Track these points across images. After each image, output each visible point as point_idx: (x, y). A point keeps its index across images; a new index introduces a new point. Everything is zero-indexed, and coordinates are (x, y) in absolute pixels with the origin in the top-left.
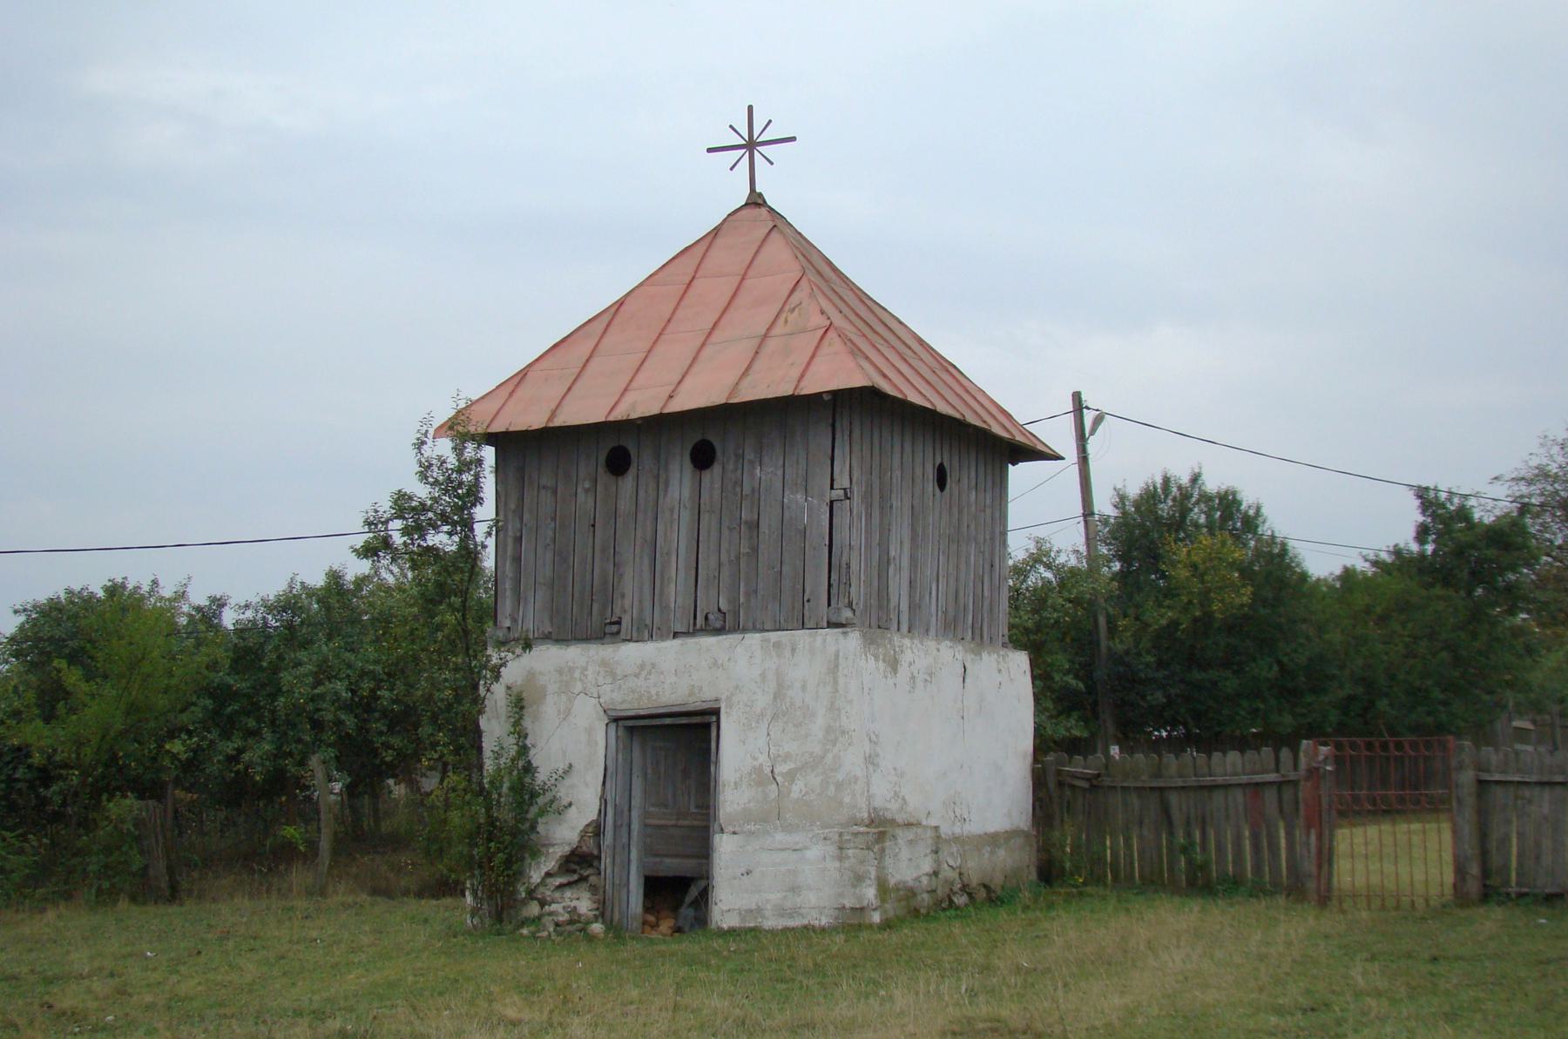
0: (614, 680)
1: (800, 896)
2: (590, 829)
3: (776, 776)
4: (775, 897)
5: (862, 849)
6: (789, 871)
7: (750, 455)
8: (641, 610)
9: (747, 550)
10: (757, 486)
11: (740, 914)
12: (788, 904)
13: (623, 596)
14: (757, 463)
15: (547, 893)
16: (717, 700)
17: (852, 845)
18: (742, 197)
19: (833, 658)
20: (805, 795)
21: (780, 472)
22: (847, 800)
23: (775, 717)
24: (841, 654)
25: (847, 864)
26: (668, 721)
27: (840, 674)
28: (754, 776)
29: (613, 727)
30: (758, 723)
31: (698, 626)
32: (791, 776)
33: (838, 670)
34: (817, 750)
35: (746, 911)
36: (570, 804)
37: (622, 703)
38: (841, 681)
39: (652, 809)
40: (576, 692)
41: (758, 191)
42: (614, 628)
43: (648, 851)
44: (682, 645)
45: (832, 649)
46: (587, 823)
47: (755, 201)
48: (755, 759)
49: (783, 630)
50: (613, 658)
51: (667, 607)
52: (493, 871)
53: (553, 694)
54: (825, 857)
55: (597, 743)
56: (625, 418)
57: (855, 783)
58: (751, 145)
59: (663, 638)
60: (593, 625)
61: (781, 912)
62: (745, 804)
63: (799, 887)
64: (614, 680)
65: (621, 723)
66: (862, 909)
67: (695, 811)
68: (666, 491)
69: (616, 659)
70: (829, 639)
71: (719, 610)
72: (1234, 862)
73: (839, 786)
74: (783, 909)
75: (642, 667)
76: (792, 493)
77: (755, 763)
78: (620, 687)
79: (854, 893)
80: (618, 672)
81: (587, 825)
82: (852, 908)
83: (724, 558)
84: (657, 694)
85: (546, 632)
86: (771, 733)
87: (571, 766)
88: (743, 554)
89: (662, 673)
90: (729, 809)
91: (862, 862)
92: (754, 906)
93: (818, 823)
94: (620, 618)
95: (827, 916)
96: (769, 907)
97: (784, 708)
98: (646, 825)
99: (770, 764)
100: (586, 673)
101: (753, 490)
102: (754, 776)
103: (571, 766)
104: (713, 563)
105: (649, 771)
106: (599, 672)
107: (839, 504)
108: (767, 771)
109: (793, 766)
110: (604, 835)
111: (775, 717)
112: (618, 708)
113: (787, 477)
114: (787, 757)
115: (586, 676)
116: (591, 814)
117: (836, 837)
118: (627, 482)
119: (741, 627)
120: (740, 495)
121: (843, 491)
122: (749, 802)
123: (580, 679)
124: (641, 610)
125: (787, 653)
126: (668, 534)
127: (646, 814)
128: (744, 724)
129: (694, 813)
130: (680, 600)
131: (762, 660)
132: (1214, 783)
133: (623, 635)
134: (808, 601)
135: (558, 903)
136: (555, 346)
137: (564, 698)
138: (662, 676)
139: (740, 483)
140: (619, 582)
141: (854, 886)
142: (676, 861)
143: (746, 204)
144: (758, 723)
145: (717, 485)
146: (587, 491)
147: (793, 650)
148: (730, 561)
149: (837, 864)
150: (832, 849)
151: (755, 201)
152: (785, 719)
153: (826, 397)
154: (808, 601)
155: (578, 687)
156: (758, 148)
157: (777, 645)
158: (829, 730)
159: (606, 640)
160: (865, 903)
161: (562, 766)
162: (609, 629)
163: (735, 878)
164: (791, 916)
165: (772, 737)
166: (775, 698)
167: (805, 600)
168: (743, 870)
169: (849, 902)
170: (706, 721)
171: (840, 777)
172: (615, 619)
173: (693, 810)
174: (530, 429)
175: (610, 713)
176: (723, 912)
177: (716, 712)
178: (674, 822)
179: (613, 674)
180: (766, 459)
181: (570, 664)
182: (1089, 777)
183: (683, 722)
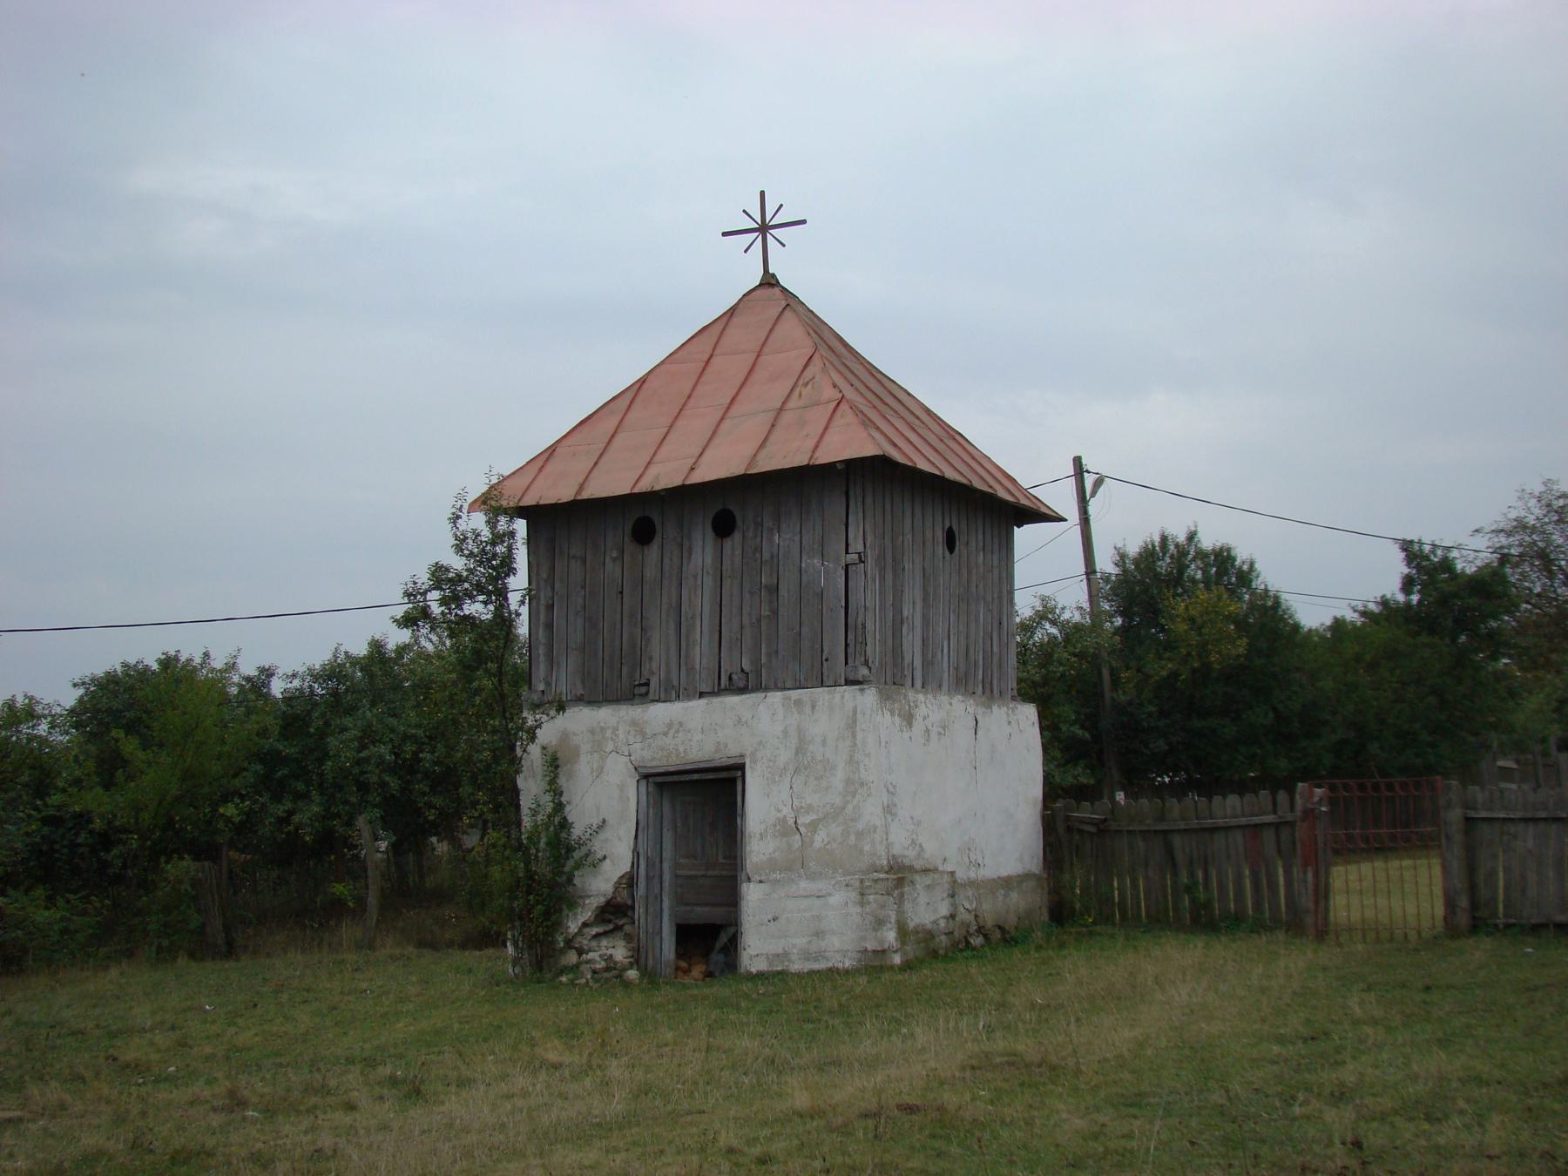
1: (823, 940)
2: (624, 881)
4: (801, 941)
5: (882, 894)
6: (813, 916)
7: (768, 523)
8: (668, 672)
9: (767, 613)
11: (768, 958)
13: (651, 659)
14: (776, 531)
15: (584, 942)
16: (742, 756)
17: (872, 891)
19: (851, 714)
20: (827, 844)
21: (797, 538)
24: (858, 711)
26: (696, 777)
27: (858, 728)
28: (778, 827)
29: (643, 783)
32: (813, 826)
34: (838, 801)
36: (605, 858)
37: (652, 760)
38: (859, 735)
40: (608, 750)
41: (771, 271)
42: (643, 690)
43: (679, 899)
45: (849, 706)
48: (779, 811)
49: (804, 688)
51: (693, 668)
55: (628, 799)
58: (764, 229)
59: (689, 697)
61: (807, 955)
66: (884, 951)
67: (724, 861)
68: (689, 563)
69: (645, 719)
71: (742, 670)
73: (859, 835)
75: (670, 726)
78: (649, 746)
83: (746, 621)
84: (685, 751)
87: (604, 821)
88: (764, 617)
90: (755, 859)
91: (882, 907)
92: (780, 951)
94: (649, 680)
95: (850, 959)
96: (795, 951)
97: (806, 762)
98: (677, 876)
99: (793, 815)
101: (772, 557)
102: (778, 827)
103: (604, 821)
108: (791, 822)
109: (815, 817)
115: (617, 736)
117: (857, 884)
118: (653, 551)
120: (759, 562)
121: (857, 555)
122: (774, 853)
123: (612, 739)
124: (668, 672)
125: (808, 709)
128: (768, 779)
133: (651, 696)
134: (827, 660)
137: (596, 756)
138: (689, 734)
140: (647, 646)
141: (875, 930)
142: (707, 909)
143: (760, 285)
145: (738, 552)
146: (614, 560)
147: (813, 707)
150: (854, 895)
151: (769, 281)
153: (839, 467)
154: (827, 660)
157: (798, 703)
158: (848, 782)
160: (886, 947)
161: (596, 822)
163: (762, 925)
164: (816, 959)
165: (795, 790)
166: (797, 753)
167: (824, 658)
169: (870, 946)
171: (860, 826)
172: (643, 681)
173: (721, 860)
178: (703, 873)
179: (642, 733)
181: (602, 724)
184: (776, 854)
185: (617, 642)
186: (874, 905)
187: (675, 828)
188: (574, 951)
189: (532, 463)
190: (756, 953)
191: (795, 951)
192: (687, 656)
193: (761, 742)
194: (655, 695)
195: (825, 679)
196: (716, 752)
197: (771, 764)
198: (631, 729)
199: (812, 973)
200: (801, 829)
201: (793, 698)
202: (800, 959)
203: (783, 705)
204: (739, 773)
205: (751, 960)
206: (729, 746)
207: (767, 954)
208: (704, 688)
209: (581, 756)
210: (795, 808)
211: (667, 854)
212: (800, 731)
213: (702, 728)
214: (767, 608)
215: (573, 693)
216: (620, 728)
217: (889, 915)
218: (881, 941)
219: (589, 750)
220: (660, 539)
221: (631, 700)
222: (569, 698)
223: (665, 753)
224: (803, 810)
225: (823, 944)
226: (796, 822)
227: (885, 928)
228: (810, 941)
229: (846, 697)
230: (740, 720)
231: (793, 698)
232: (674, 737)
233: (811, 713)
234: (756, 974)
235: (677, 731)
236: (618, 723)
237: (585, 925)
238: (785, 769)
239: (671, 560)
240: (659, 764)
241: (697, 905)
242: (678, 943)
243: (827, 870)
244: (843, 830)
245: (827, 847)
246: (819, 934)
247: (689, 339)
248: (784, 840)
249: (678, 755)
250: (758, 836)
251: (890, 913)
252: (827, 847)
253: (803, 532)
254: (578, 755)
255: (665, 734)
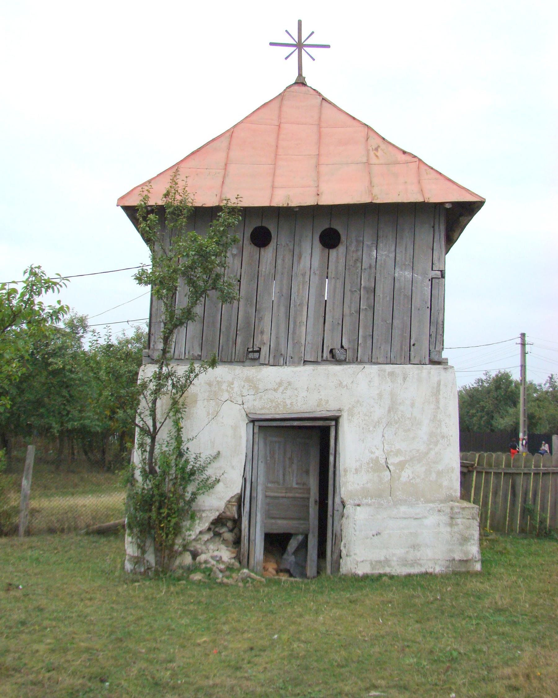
0: (257, 393)
1: (419, 551)
2: (234, 500)
3: (389, 466)
4: (400, 552)
5: (469, 519)
6: (411, 533)
7: (368, 242)
8: (278, 344)
9: (364, 308)
10: (373, 264)
11: (371, 564)
12: (410, 557)
13: (262, 333)
14: (374, 248)
15: (199, 547)
16: (340, 410)
17: (461, 516)
18: (293, 78)
19: (435, 385)
20: (411, 479)
21: (392, 255)
22: (445, 483)
23: (389, 424)
24: (442, 383)
25: (456, 529)
26: (296, 423)
27: (441, 397)
28: (371, 465)
29: (251, 425)
30: (375, 427)
31: (324, 358)
32: (402, 465)
33: (439, 394)
34: (423, 448)
35: (376, 562)
36: (218, 481)
37: (261, 409)
38: (442, 402)
39: (269, 485)
40: (223, 399)
41: (303, 75)
42: (256, 355)
43: (268, 515)
44: (314, 370)
45: (435, 379)
46: (233, 495)
47: (301, 82)
48: (372, 453)
49: (392, 364)
50: (256, 376)
51: (299, 342)
52: (163, 531)
53: (204, 400)
54: (439, 524)
55: (241, 437)
56: (285, 205)
57: (452, 472)
58: (300, 46)
59: (298, 364)
60: (237, 352)
61: (404, 562)
62: (363, 485)
63: (418, 545)
64: (257, 393)
65: (256, 423)
66: (466, 561)
67: (296, 486)
68: (299, 262)
69: (258, 377)
70: (433, 372)
71: (342, 347)
72: (551, 519)
73: (440, 474)
74: (406, 561)
75: (280, 384)
76: (401, 270)
77: (372, 456)
78: (261, 398)
79: (462, 549)
80: (260, 387)
81: (232, 497)
82: (460, 561)
83: (346, 310)
84: (291, 404)
85: (196, 354)
86: (386, 435)
87: (219, 453)
88: (363, 309)
89: (296, 389)
90: (350, 488)
91: (468, 528)
92: (382, 558)
93: (422, 499)
94: (260, 348)
95: (440, 565)
96: (395, 559)
97: (396, 418)
98: (266, 497)
99: (384, 457)
100: (232, 386)
101: (370, 267)
102: (371, 465)
103: (219, 453)
104: (338, 315)
105: (268, 458)
106: (244, 386)
107: (437, 281)
108: (383, 461)
109: (402, 458)
110: (244, 504)
111: (389, 424)
112: (258, 412)
113: (397, 259)
114: (398, 452)
115: (232, 388)
116: (237, 490)
117: (448, 510)
118: (268, 253)
119: (359, 360)
120: (360, 268)
121: (439, 272)
122: (367, 483)
123: (227, 391)
124: (278, 344)
125: (400, 380)
126: (301, 292)
127: (266, 489)
128: (363, 429)
129: (297, 488)
130: (309, 338)
131: (380, 384)
132: (547, 471)
133: (262, 360)
134: (414, 345)
135: (205, 553)
136: (193, 153)
137: (213, 403)
138: (295, 391)
139: (360, 260)
140: (260, 321)
141: (461, 544)
142: (285, 522)
143: (296, 83)
144: (375, 427)
145: (342, 261)
146: (234, 256)
147: (405, 379)
148: (351, 314)
149: (449, 529)
150: (445, 519)
151: (301, 82)
152: (397, 426)
153: (448, 206)
154: (414, 345)
155: (226, 396)
156: (297, 50)
157: (391, 374)
158: (432, 435)
159: (246, 364)
160: (470, 557)
161: (214, 453)
162: (251, 355)
163: (367, 538)
164: (412, 565)
165: (386, 438)
166: (389, 411)
167: (412, 344)
168: (374, 532)
169: (458, 556)
170: (327, 425)
171: (440, 467)
172: (256, 349)
173: (295, 486)
174: (204, 206)
175: (251, 416)
176: (357, 562)
177: (336, 419)
178: (283, 495)
179: (256, 389)
180: (381, 245)
181: (219, 379)
182: (468, 465)
183: (309, 424)
184: (369, 484)
185: (234, 318)
186: (461, 527)
187: (266, 463)
188: (188, 553)
189: (162, 175)
190: (362, 559)
191: (395, 559)
192: (294, 333)
193: (358, 401)
194: (265, 359)
195: (412, 358)
196: (318, 406)
197: (367, 418)
198: (246, 384)
199: (409, 576)
200: (390, 467)
201: (387, 371)
202: (398, 565)
203: (379, 375)
204: (333, 423)
205: (357, 564)
206: (329, 403)
207: (371, 561)
208: (308, 358)
209: (198, 402)
210: (386, 451)
211: (261, 480)
212: (393, 395)
213: (308, 388)
214: (365, 304)
215: (191, 353)
216: (235, 382)
217: (473, 535)
218: (466, 553)
219: (206, 398)
220: (275, 244)
221: (243, 362)
222: (187, 357)
223: (274, 404)
224: (392, 453)
225: (418, 554)
226: (386, 462)
227: (469, 543)
228: (407, 552)
229: (432, 373)
230: (340, 384)
231: (387, 371)
232: (282, 393)
233: (402, 382)
234: (362, 577)
235: (286, 389)
236: (233, 379)
237: (201, 533)
238: (379, 422)
239: (283, 261)
240: (267, 412)
241: (279, 518)
242: (266, 549)
243: (411, 498)
244: (426, 470)
245: (412, 481)
246: (415, 547)
247: (254, 112)
248: (376, 474)
249: (285, 405)
250: (353, 471)
251: (474, 532)
252: (412, 481)
253: (397, 251)
254: (196, 401)
255: (275, 390)
